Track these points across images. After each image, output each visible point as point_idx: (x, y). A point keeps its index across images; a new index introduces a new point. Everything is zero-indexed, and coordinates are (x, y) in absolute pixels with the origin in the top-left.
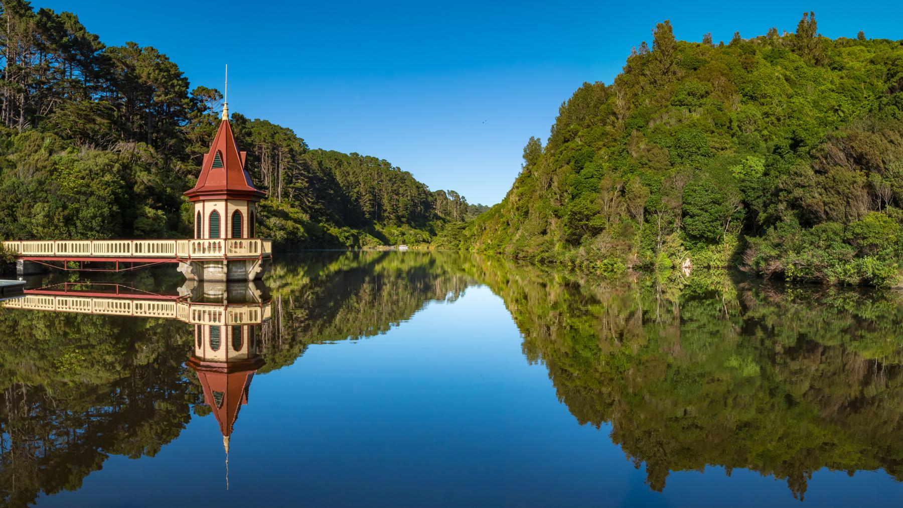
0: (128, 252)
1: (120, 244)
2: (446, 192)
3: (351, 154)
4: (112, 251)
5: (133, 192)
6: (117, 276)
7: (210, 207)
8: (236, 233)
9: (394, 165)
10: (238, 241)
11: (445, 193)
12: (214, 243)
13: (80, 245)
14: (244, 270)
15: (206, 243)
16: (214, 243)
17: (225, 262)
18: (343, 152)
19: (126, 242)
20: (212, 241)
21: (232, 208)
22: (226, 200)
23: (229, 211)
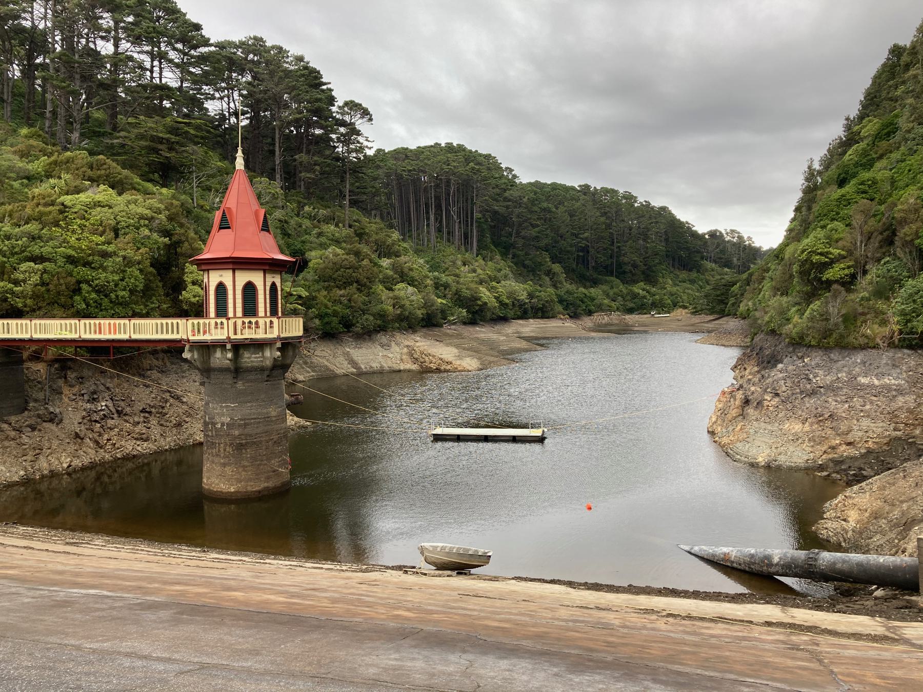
0: (125, 333)
1: (167, 324)
2: (723, 232)
3: (580, 186)
4: (162, 333)
5: (777, 254)
6: (405, 376)
7: (214, 278)
8: (250, 309)
9: (641, 199)
10: (253, 320)
11: (721, 233)
12: (250, 322)
13: (95, 324)
14: (261, 354)
15: (213, 322)
16: (250, 322)
17: (229, 346)
18: (569, 184)
19: (175, 321)
20: (247, 320)
21: (270, 279)
22: (234, 271)
23: (237, 283)
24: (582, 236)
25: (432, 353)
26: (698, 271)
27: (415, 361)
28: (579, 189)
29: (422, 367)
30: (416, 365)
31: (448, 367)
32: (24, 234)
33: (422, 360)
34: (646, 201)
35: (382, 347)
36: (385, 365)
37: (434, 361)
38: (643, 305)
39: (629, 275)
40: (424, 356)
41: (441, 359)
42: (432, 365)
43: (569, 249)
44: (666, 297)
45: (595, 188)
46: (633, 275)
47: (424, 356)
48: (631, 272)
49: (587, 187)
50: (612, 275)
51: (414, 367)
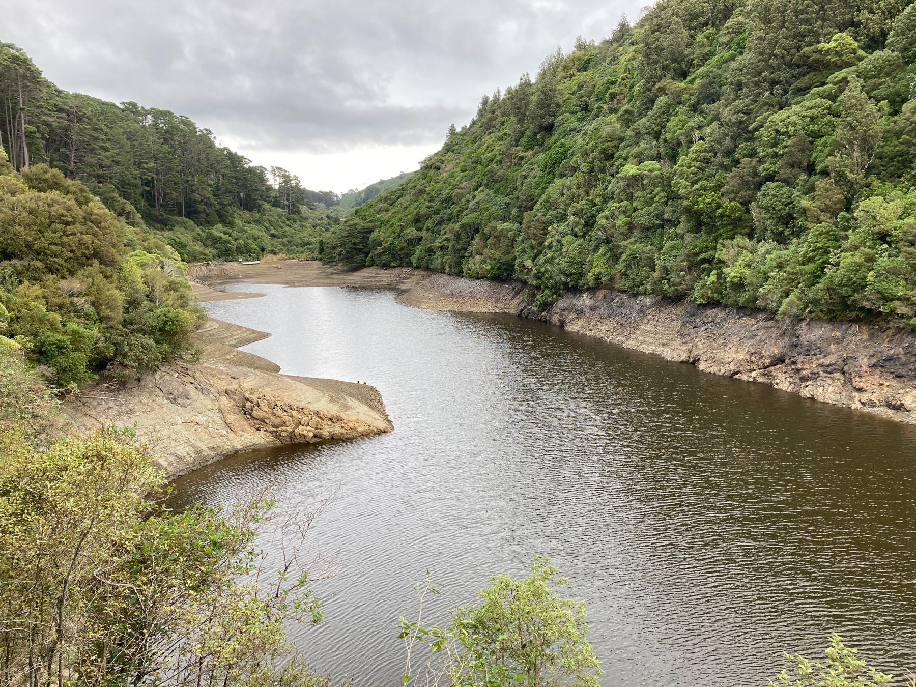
3: (123, 103)
24: (145, 166)
25: (295, 404)
26: (259, 211)
27: (259, 423)
28: (122, 107)
29: (277, 436)
30: (262, 433)
31: (337, 429)
32: (623, 149)
33: (277, 421)
34: (206, 130)
35: (174, 401)
36: (202, 446)
37: (305, 419)
38: (226, 251)
39: (203, 215)
40: (280, 413)
41: (317, 414)
42: (301, 430)
43: (133, 181)
44: (250, 241)
45: (142, 107)
46: (208, 215)
47: (280, 413)
48: (205, 212)
49: (133, 105)
50: (180, 214)
51: (261, 439)
